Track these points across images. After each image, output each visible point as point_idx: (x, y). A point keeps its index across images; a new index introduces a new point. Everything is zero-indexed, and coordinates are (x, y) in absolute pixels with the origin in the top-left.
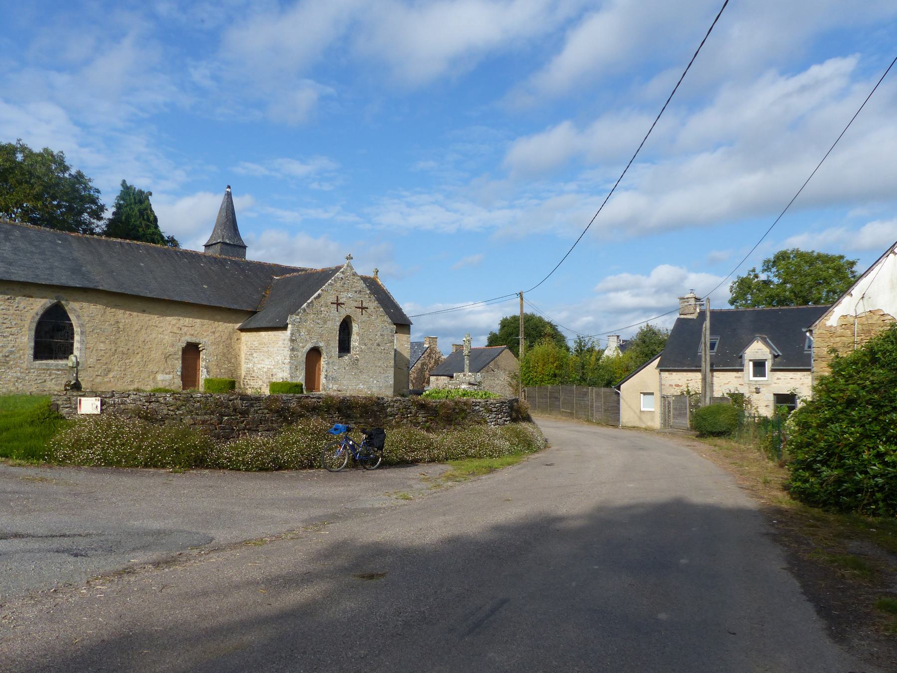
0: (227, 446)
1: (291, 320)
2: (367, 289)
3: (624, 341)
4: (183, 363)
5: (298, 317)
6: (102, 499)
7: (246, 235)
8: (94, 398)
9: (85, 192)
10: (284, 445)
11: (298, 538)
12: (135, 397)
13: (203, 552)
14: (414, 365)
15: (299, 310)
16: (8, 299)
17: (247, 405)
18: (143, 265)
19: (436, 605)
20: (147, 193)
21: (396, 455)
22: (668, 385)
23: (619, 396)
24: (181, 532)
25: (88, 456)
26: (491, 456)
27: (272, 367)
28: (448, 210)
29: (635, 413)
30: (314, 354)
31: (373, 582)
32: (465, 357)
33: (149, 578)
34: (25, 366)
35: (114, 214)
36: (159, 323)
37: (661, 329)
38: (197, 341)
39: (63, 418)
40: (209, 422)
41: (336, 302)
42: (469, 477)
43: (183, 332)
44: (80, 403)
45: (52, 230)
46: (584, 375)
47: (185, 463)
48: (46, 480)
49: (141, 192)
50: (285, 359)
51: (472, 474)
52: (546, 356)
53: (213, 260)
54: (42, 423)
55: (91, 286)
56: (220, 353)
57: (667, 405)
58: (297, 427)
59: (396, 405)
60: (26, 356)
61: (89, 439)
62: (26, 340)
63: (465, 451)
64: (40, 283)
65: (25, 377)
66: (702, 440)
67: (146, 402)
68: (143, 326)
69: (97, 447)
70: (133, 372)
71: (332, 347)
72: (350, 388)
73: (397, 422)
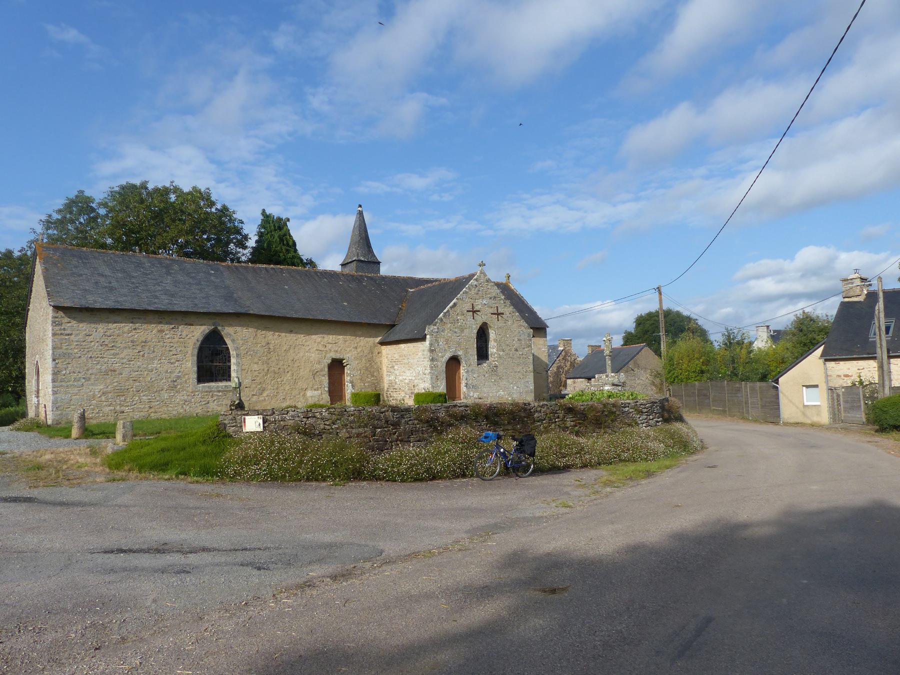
0: (381, 458)
1: (429, 330)
2: (501, 295)
3: (775, 331)
4: (329, 379)
5: (435, 327)
6: (273, 513)
7: (379, 252)
8: (256, 417)
9: (230, 224)
10: (436, 455)
11: (465, 550)
12: (293, 413)
13: (375, 565)
14: (550, 368)
15: (436, 320)
16: (173, 328)
17: (397, 416)
18: (287, 287)
19: (633, 624)
21: (547, 461)
22: (835, 376)
23: (778, 390)
24: (351, 544)
25: (255, 472)
26: (646, 460)
27: (413, 378)
28: (571, 209)
29: (798, 408)
30: (454, 362)
31: (556, 596)
32: (607, 357)
33: (329, 592)
34: (190, 389)
35: (256, 242)
36: (306, 341)
37: (820, 315)
38: (341, 357)
39: (230, 436)
40: (363, 435)
42: (627, 482)
43: (327, 349)
44: (245, 422)
45: (205, 262)
46: (735, 369)
47: (344, 476)
48: (222, 495)
49: (280, 219)
50: (425, 370)
51: (629, 478)
52: (691, 351)
53: (350, 278)
54: (212, 441)
56: (363, 367)
57: (835, 398)
58: (447, 436)
59: (543, 410)
60: (191, 380)
61: (255, 456)
62: (190, 366)
63: (617, 455)
64: (199, 311)
65: (191, 400)
66: (884, 435)
67: (304, 418)
69: (263, 463)
72: (491, 395)
73: (545, 428)
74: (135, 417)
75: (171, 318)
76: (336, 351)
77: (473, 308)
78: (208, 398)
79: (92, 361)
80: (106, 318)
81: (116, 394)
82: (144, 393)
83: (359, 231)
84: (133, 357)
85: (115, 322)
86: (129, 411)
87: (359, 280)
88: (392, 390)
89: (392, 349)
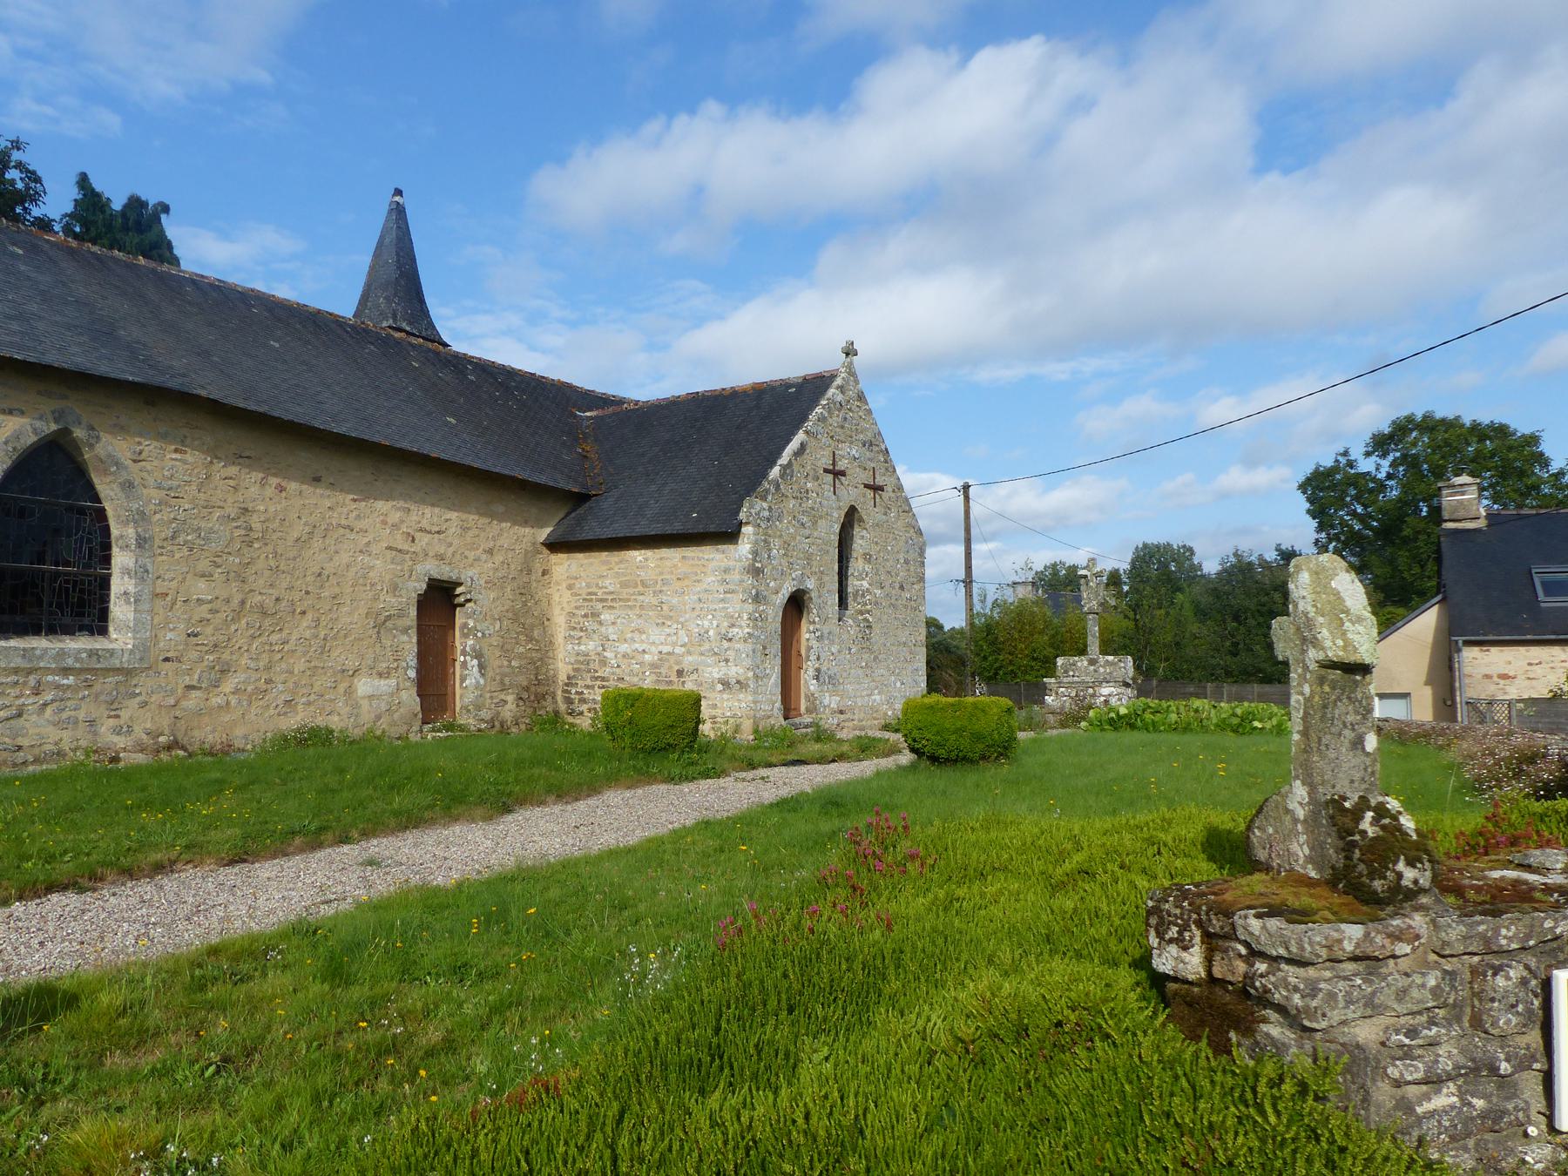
4: (419, 642)
5: (765, 505)
15: (766, 485)
20: (154, 206)
22: (1480, 676)
27: (678, 650)
30: (797, 604)
36: (358, 517)
41: (831, 467)
49: (135, 203)
50: (733, 626)
55: (174, 384)
68: (315, 526)
70: (292, 673)
76: (440, 557)
77: (834, 464)
78: (21, 696)
83: (398, 254)
88: (589, 682)
89: (591, 564)
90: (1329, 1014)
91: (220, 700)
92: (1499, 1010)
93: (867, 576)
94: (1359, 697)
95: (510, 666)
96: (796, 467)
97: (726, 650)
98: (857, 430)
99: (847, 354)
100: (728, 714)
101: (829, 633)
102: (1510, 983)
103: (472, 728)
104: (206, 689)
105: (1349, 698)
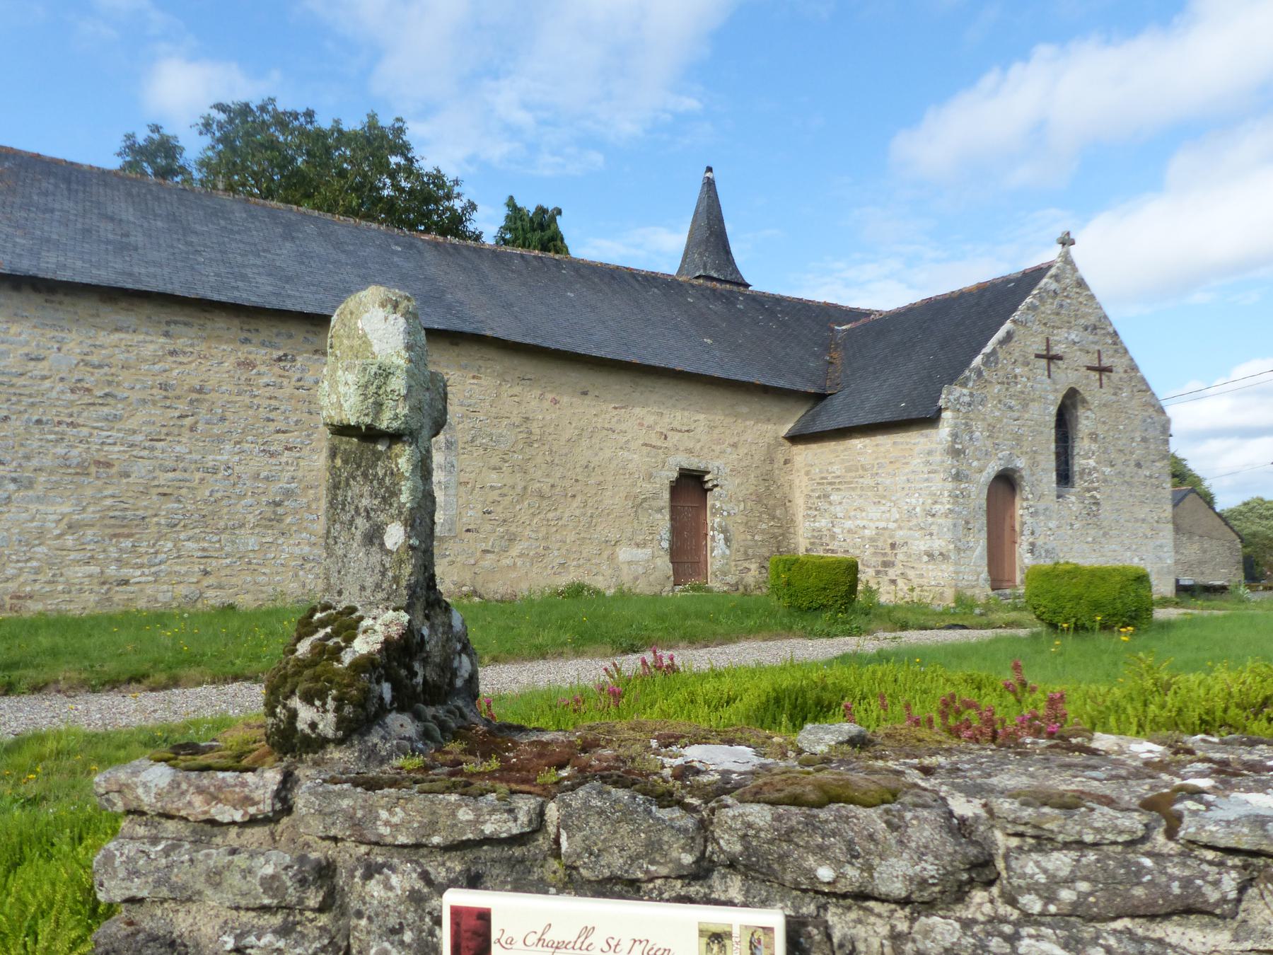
1: (951, 397)
4: (672, 519)
5: (965, 391)
15: (967, 373)
16: (280, 359)
27: (892, 525)
30: (1006, 482)
38: (702, 467)
41: (1045, 353)
49: (541, 211)
50: (935, 502)
55: (467, 328)
70: (565, 542)
71: (1043, 470)
74: (161, 597)
75: (275, 330)
77: (1048, 349)
79: (42, 432)
80: (92, 316)
81: (110, 531)
82: (190, 533)
83: (708, 218)
84: (164, 430)
85: (117, 330)
86: (143, 579)
87: (727, 299)
90: (106, 884)
91: (508, 562)
92: (369, 933)
93: (1093, 454)
94: (380, 474)
95: (753, 540)
96: (1001, 355)
97: (931, 525)
98: (1076, 315)
99: (1064, 244)
100: (933, 583)
101: (1046, 509)
102: (391, 894)
103: (715, 589)
104: (498, 553)
105: (365, 475)
